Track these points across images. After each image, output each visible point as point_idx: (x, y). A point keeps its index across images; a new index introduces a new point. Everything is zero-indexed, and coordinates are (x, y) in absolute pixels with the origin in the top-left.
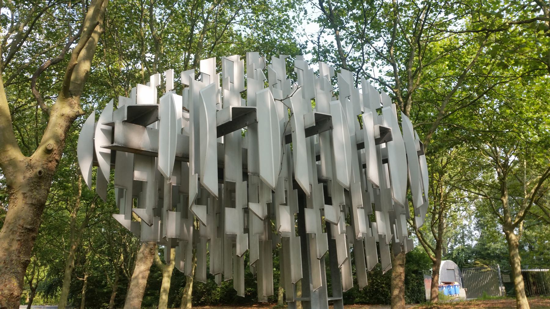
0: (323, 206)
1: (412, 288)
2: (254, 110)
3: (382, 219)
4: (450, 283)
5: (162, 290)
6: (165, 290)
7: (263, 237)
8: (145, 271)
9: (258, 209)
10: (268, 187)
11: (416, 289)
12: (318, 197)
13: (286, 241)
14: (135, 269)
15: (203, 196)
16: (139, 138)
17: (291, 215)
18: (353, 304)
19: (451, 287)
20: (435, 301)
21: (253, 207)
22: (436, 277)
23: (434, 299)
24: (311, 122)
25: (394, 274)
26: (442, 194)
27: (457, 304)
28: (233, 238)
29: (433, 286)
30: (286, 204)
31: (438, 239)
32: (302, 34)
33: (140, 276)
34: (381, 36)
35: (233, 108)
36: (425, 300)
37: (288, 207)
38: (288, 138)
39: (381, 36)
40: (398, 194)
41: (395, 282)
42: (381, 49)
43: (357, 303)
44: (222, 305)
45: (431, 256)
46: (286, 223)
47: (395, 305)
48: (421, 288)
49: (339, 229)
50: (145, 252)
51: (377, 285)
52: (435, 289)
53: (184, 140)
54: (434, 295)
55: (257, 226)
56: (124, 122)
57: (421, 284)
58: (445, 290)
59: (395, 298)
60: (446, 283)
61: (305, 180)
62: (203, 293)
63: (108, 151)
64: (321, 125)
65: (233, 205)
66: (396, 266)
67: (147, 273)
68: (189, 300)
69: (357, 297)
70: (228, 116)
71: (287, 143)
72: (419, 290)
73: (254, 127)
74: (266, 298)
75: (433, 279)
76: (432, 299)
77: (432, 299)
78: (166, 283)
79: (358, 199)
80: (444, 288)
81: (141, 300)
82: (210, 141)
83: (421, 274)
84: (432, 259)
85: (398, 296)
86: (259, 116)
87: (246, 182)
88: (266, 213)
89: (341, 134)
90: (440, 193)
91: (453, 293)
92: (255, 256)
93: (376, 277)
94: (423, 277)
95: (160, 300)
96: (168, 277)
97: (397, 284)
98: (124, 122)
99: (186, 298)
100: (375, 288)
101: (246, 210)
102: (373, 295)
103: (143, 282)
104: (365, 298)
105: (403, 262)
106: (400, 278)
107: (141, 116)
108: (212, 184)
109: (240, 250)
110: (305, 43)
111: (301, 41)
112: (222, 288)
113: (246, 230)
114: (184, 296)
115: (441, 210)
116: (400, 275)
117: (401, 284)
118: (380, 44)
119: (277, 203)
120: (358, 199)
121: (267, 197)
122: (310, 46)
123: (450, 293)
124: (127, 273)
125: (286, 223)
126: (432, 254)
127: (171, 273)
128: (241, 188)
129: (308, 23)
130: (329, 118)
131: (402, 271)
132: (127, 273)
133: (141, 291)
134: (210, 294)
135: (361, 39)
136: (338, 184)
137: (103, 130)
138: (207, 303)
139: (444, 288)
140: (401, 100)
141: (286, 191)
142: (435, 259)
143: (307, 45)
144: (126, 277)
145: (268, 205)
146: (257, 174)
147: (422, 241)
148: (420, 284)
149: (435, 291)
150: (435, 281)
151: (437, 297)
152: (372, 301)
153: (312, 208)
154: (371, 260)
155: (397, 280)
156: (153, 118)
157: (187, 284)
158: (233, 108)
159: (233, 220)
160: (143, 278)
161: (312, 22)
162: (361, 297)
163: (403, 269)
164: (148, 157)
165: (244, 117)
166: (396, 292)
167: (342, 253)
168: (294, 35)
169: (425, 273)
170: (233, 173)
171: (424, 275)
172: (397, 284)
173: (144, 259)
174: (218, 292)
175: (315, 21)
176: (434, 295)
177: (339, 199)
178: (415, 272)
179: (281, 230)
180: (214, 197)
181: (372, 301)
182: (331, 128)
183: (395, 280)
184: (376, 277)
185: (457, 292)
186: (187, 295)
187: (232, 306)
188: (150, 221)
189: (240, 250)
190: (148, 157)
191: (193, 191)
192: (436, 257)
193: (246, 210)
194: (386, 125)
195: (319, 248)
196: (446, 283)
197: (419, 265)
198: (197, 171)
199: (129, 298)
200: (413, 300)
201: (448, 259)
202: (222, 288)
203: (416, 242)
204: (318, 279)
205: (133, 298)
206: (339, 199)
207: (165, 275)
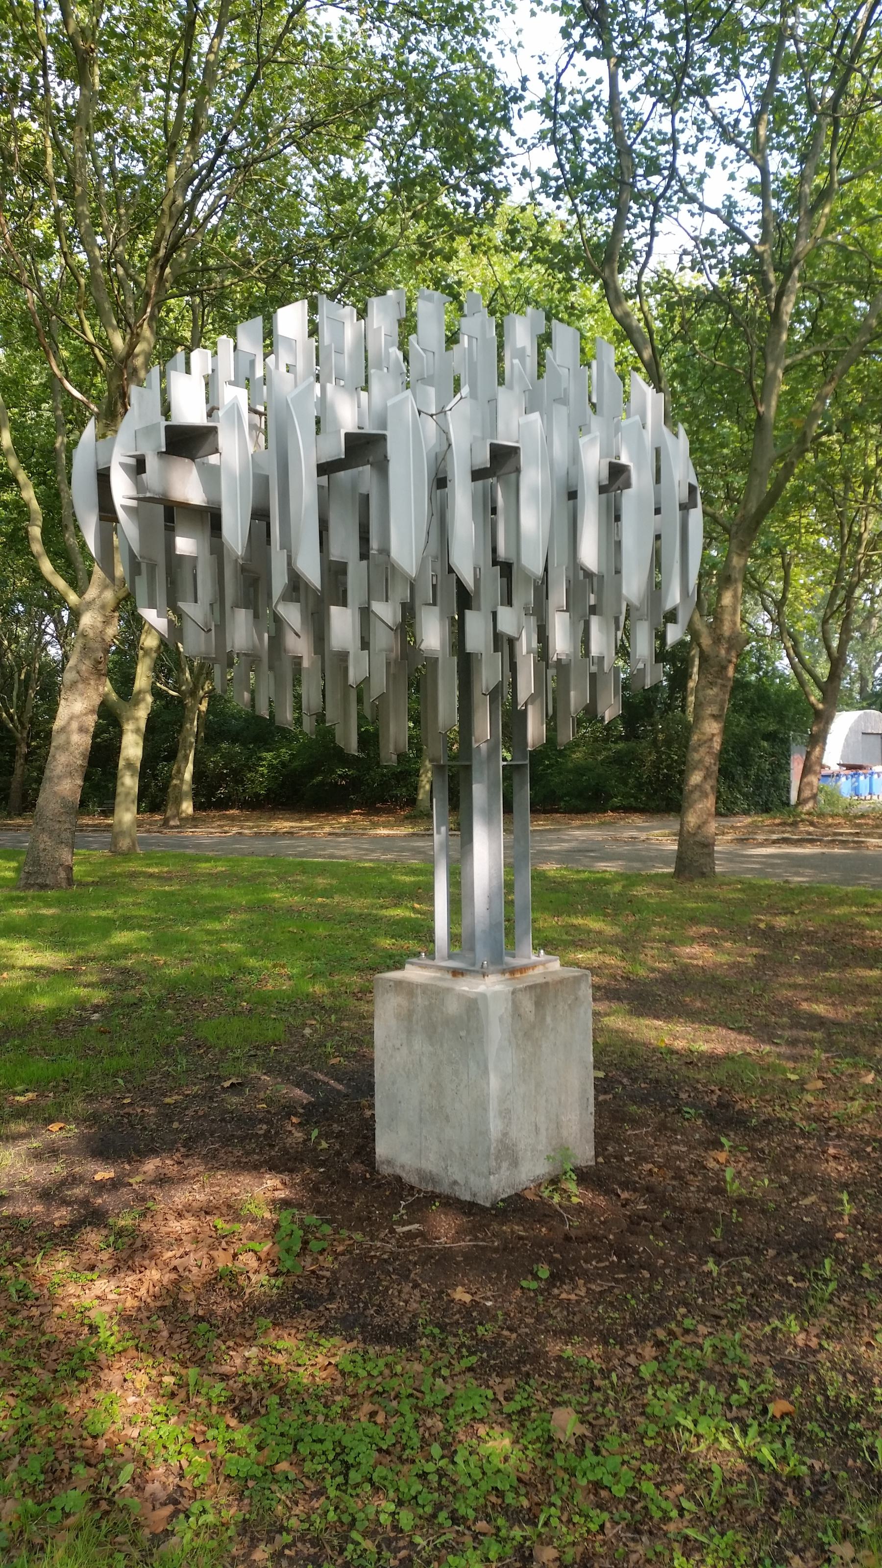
0: (496, 606)
1: (757, 776)
2: (383, 438)
3: (600, 630)
4: (860, 767)
5: (122, 763)
6: (129, 765)
7: (393, 655)
8: (86, 714)
9: (386, 612)
10: (405, 577)
11: (768, 777)
12: (491, 588)
13: (432, 662)
14: (61, 709)
15: (296, 585)
16: (188, 486)
17: (442, 619)
18: (605, 811)
19: (862, 778)
20: (809, 806)
21: (379, 608)
22: (818, 749)
23: (806, 801)
24: (484, 458)
25: (695, 738)
26: (866, 536)
27: (862, 816)
28: (343, 657)
29: (806, 770)
30: (434, 604)
31: (836, 654)
32: (515, 44)
33: (75, 725)
34: (738, 76)
35: (347, 435)
36: (787, 804)
37: (436, 609)
38: (441, 482)
39: (738, 76)
40: (633, 585)
41: (696, 756)
42: (735, 115)
43: (614, 809)
44: (272, 809)
45: (813, 699)
46: (432, 636)
47: (691, 806)
48: (781, 777)
49: (527, 644)
50: (84, 668)
51: (669, 767)
52: (813, 779)
53: (262, 483)
54: (807, 793)
55: (383, 639)
56: (160, 453)
57: (784, 767)
58: (845, 785)
59: (692, 792)
60: (849, 767)
61: (466, 559)
62: (222, 777)
63: (134, 503)
64: (502, 461)
65: (343, 602)
66: (703, 719)
67: (91, 721)
68: (186, 794)
69: (616, 796)
70: (337, 449)
71: (439, 487)
72: (775, 780)
73: (382, 467)
74: (394, 757)
75: (808, 754)
76: (801, 802)
77: (801, 802)
78: (132, 748)
79: (558, 596)
80: (843, 779)
81: (80, 782)
82: (305, 487)
83: (785, 741)
84: (812, 705)
85: (697, 786)
86: (393, 449)
87: (365, 562)
88: (399, 619)
89: (533, 478)
90: (861, 535)
91: (864, 791)
92: (379, 685)
93: (669, 748)
94: (788, 750)
95: (120, 789)
96: (137, 731)
97: (701, 761)
98: (160, 453)
99: (180, 789)
100: (664, 775)
101: (365, 613)
102: (656, 791)
103: (81, 742)
104: (636, 798)
105: (722, 709)
106: (710, 747)
107: (186, 442)
108: (310, 569)
109: (354, 677)
110: (518, 85)
111: (508, 78)
112: (271, 767)
113: (365, 644)
114: (175, 782)
115: (856, 579)
116: (711, 740)
117: (709, 760)
118: (733, 100)
119: (418, 603)
120: (558, 596)
121: (401, 593)
122: (536, 91)
123: (856, 791)
124: (12, 720)
125: (432, 636)
126: (815, 696)
127: (143, 724)
128: (356, 576)
129: (533, 14)
130: (513, 452)
131: (715, 731)
132: (12, 720)
133: (79, 762)
134: (240, 782)
135: (678, 87)
136: (522, 569)
137: (122, 465)
138: (234, 802)
139: (843, 779)
140: (772, 277)
141: (434, 587)
142: (821, 706)
143: (524, 89)
144: (9, 730)
145: (403, 605)
146: (385, 551)
147: (799, 664)
148: (779, 765)
149: (810, 784)
150: (813, 758)
151: (814, 797)
152: (653, 805)
153: (479, 609)
154: (577, 699)
155: (703, 750)
156: (206, 447)
157: (180, 755)
158: (347, 435)
159: (342, 623)
160: (82, 730)
161: (546, 10)
162: (626, 796)
163: (721, 725)
164: (209, 518)
165: (365, 448)
166: (696, 778)
167: (526, 685)
168: (489, 45)
169: (794, 739)
170: (344, 546)
171: (793, 746)
172: (701, 761)
173: (80, 686)
174: (262, 775)
175: (554, 9)
176: (807, 793)
177: (524, 596)
178: (770, 737)
179: (423, 647)
180: (315, 591)
181: (653, 805)
182: (518, 470)
183: (697, 751)
184: (669, 748)
185: (874, 790)
186: (182, 780)
187: (299, 812)
188: (206, 624)
189: (354, 677)
190: (209, 518)
191: (279, 581)
192: (824, 700)
193: (365, 613)
194: (624, 460)
195: (488, 675)
196: (849, 767)
197: (781, 719)
198: (286, 544)
199: (50, 779)
200: (757, 804)
201: (869, 707)
202: (271, 767)
203: (783, 664)
204: (484, 728)
205: (59, 777)
206: (524, 596)
207: (129, 727)
